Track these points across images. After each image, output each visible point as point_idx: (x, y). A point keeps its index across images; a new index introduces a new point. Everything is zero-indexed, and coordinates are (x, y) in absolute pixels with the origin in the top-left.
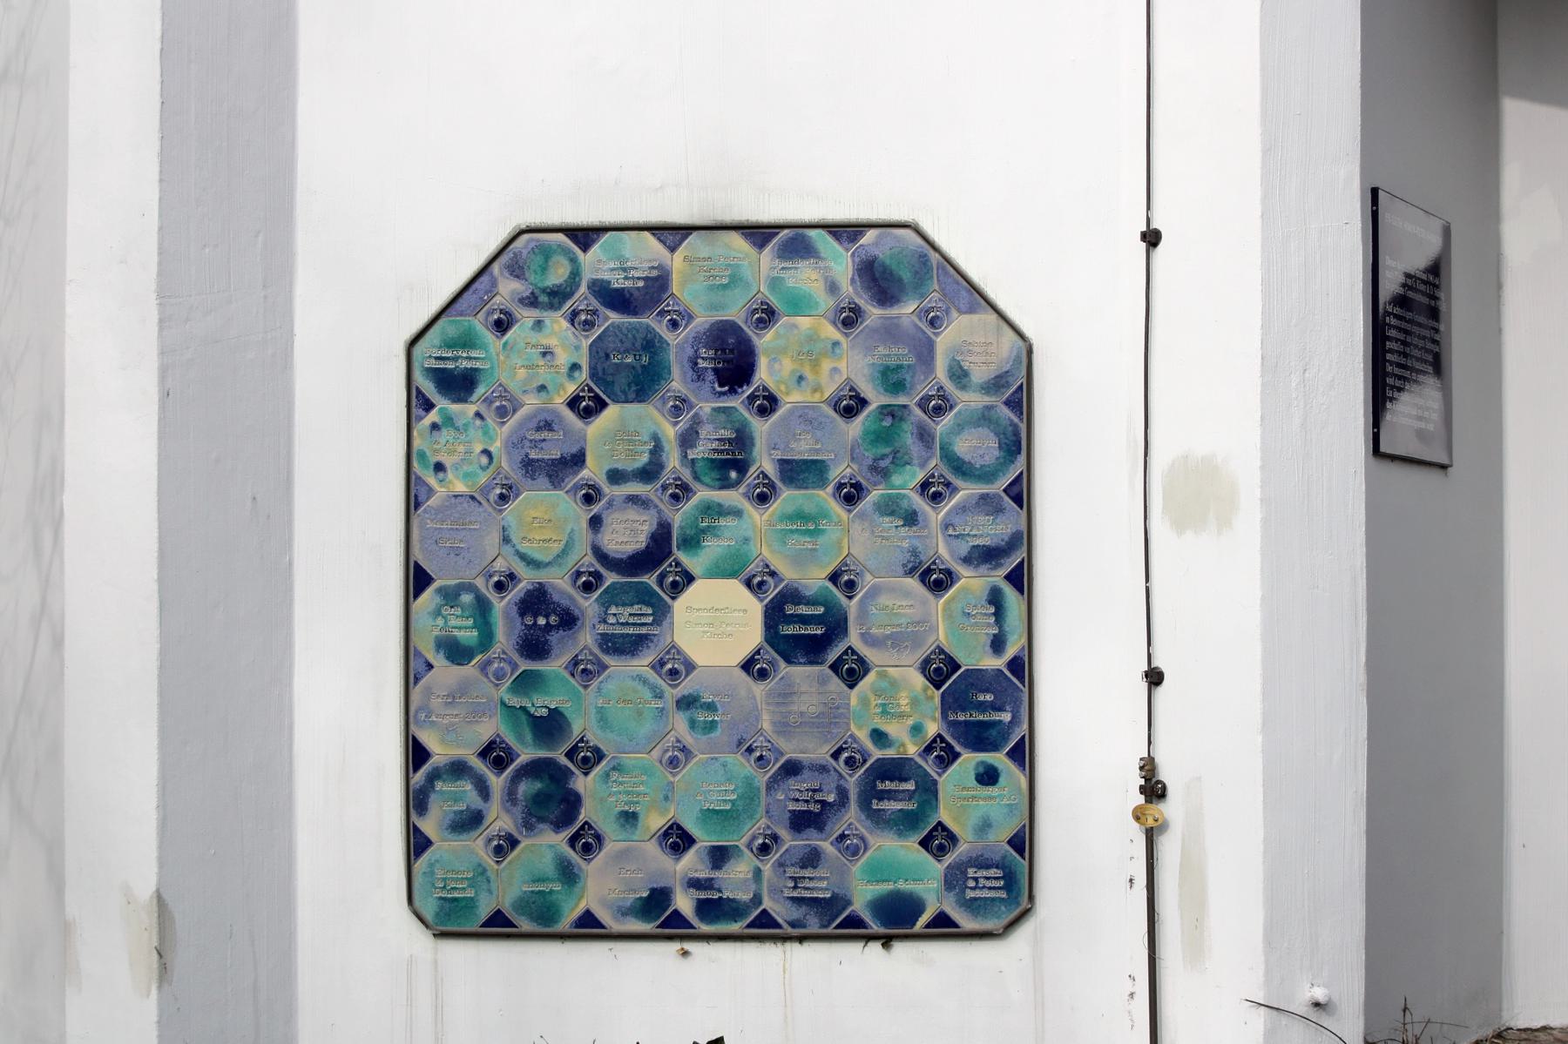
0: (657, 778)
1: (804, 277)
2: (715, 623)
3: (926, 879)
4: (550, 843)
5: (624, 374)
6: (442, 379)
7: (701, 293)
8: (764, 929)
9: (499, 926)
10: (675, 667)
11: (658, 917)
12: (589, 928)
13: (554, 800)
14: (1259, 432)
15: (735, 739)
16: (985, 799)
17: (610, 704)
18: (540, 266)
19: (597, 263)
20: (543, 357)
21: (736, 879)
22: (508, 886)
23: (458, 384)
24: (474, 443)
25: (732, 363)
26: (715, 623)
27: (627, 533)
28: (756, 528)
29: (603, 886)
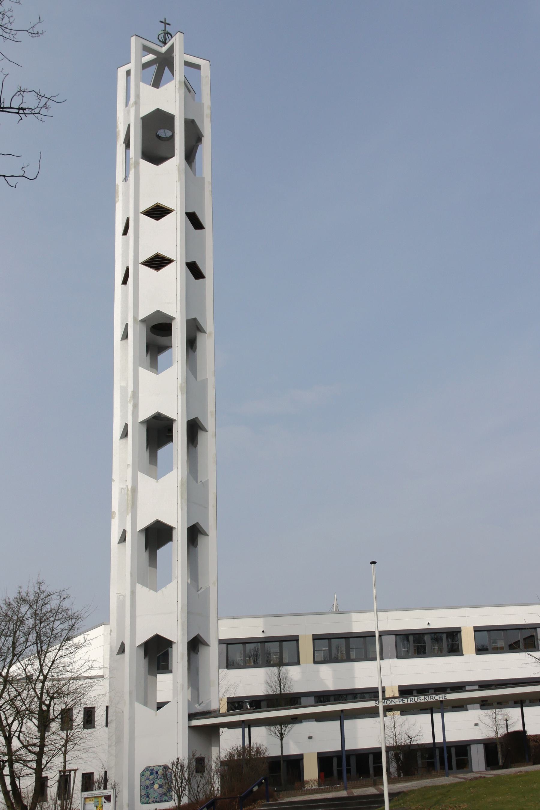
0: (153, 795)
1: (161, 768)
2: (156, 786)
3: (167, 798)
4: (147, 799)
5: (151, 774)
6: (142, 775)
7: (155, 769)
8: (159, 802)
9: (145, 803)
10: (154, 789)
11: (153, 802)
12: (150, 803)
13: (148, 796)
14: (12, 741)
15: (311, 740)
16: (446, 642)
17: (151, 791)
18: (147, 769)
19: (150, 768)
20: (148, 773)
21: (157, 800)
22: (146, 801)
23: (143, 775)
24: (144, 778)
25: (157, 773)
26: (156, 786)
27: (152, 782)
28: (158, 781)
29: (150, 801)
